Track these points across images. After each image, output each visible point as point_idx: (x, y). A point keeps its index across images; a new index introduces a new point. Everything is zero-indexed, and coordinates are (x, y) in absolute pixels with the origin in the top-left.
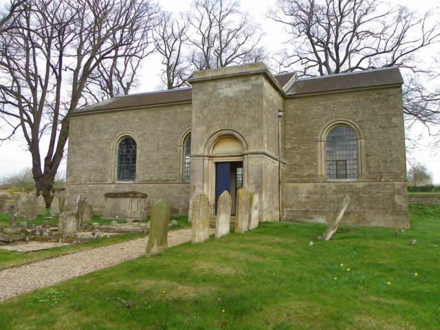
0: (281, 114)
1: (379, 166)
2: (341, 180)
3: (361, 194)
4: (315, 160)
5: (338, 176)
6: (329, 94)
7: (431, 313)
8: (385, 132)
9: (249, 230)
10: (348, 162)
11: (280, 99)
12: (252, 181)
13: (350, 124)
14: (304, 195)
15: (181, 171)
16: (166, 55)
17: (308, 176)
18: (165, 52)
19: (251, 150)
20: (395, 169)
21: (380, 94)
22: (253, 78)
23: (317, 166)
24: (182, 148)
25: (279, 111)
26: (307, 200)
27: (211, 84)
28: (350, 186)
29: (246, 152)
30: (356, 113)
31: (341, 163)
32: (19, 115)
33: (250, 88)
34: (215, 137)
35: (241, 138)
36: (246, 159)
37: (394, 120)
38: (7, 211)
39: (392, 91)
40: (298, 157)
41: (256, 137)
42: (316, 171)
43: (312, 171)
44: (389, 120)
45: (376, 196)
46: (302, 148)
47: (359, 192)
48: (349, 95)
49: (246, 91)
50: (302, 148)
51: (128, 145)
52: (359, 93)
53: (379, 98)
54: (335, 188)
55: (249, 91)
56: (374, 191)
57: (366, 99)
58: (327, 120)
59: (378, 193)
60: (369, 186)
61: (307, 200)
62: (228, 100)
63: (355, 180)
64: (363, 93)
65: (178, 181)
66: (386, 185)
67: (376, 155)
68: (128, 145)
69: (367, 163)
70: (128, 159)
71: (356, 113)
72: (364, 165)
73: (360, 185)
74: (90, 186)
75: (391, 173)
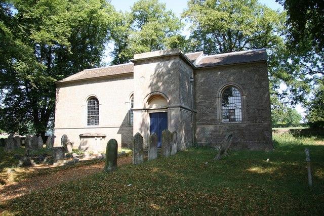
0: (192, 80)
2: (232, 123)
7: (221, 167)
8: (258, 91)
9: (170, 156)
11: (191, 71)
14: (208, 133)
17: (212, 120)
23: (216, 114)
25: (191, 78)
26: (210, 136)
29: (169, 106)
35: (164, 96)
36: (169, 111)
37: (263, 83)
38: (42, 32)
40: (204, 108)
41: (175, 96)
42: (217, 117)
43: (214, 117)
45: (253, 132)
50: (207, 102)
51: (93, 100)
54: (228, 127)
56: (252, 129)
61: (210, 136)
66: (259, 124)
68: (93, 100)
70: (93, 109)
71: (240, 79)
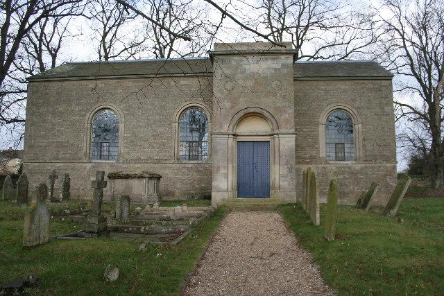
1: (373, 150)
3: (359, 175)
4: (316, 142)
5: (337, 158)
6: (306, 80)
8: (378, 119)
10: (346, 145)
12: (283, 162)
13: (348, 110)
15: (176, 150)
16: (103, 22)
18: (102, 18)
19: (282, 131)
20: (387, 153)
21: (374, 84)
22: (283, 57)
24: (177, 124)
27: (236, 58)
28: (349, 168)
30: (354, 100)
31: (340, 146)
32: (412, 73)
33: (280, 66)
34: (242, 114)
37: (386, 109)
39: (384, 83)
42: (318, 152)
44: (382, 108)
46: (305, 130)
47: (357, 173)
48: (347, 83)
49: (276, 70)
50: (305, 130)
52: (356, 81)
53: (374, 88)
55: (279, 69)
57: (362, 88)
58: (328, 105)
59: (374, 174)
60: (366, 167)
62: (252, 76)
63: (354, 162)
64: (360, 82)
65: (173, 161)
67: (371, 140)
69: (364, 146)
72: (361, 148)
73: (358, 167)
74: (58, 165)
75: (383, 156)
